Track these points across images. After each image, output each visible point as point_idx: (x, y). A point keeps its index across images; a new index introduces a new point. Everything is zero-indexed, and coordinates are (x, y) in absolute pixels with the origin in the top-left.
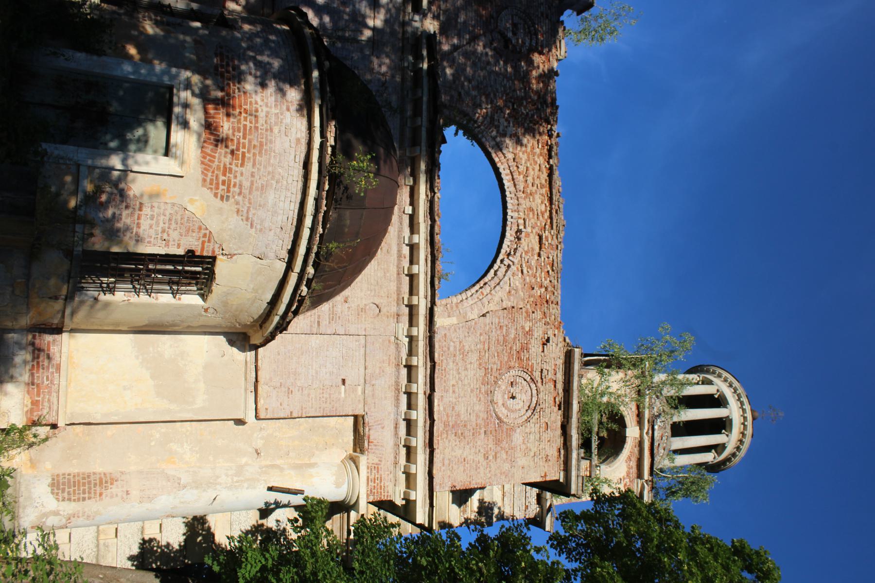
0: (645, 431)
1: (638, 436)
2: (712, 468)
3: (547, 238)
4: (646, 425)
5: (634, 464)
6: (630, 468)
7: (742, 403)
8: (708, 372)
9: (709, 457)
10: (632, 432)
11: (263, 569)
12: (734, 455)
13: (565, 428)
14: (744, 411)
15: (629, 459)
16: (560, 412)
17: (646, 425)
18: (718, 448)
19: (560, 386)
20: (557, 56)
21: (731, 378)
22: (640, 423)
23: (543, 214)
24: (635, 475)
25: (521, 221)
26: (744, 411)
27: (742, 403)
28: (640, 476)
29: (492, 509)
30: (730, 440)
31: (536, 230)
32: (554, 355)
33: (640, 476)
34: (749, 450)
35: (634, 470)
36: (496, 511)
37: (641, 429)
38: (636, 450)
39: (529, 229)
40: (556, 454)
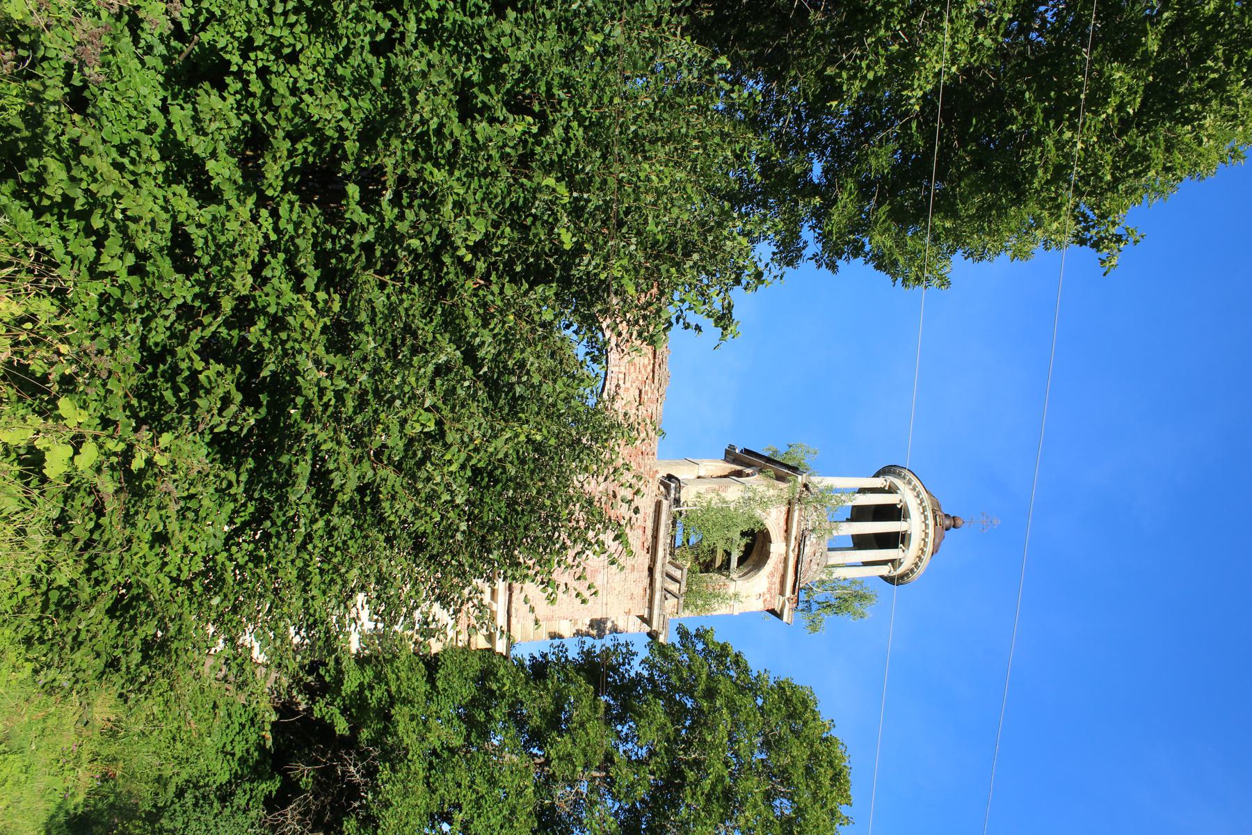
0: (792, 547)
1: (783, 552)
2: (889, 580)
3: (646, 393)
4: (793, 543)
5: (777, 580)
6: (772, 583)
7: (926, 518)
8: (899, 475)
9: (885, 570)
10: (777, 548)
11: (361, 685)
12: (912, 571)
13: (651, 570)
14: (927, 526)
15: (772, 574)
16: (648, 556)
17: (793, 543)
18: (893, 562)
19: (649, 532)
20: (128, 519)
21: (920, 488)
22: (787, 539)
23: (645, 367)
24: (777, 592)
25: (621, 376)
26: (927, 526)
27: (926, 518)
28: (782, 593)
29: (605, 623)
30: (907, 556)
31: (637, 383)
32: (163, 745)
33: (782, 593)
34: (927, 570)
35: (777, 586)
36: (609, 625)
37: (788, 545)
38: (781, 566)
39: (628, 384)
40: (642, 592)
